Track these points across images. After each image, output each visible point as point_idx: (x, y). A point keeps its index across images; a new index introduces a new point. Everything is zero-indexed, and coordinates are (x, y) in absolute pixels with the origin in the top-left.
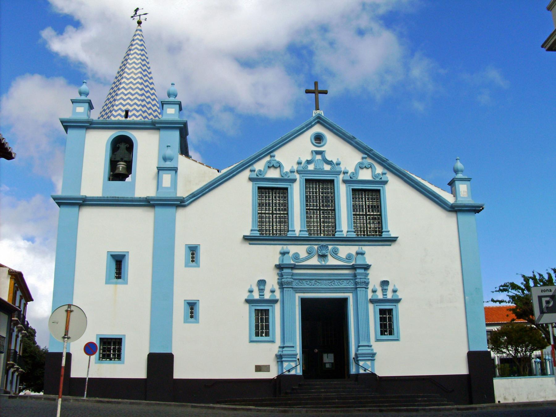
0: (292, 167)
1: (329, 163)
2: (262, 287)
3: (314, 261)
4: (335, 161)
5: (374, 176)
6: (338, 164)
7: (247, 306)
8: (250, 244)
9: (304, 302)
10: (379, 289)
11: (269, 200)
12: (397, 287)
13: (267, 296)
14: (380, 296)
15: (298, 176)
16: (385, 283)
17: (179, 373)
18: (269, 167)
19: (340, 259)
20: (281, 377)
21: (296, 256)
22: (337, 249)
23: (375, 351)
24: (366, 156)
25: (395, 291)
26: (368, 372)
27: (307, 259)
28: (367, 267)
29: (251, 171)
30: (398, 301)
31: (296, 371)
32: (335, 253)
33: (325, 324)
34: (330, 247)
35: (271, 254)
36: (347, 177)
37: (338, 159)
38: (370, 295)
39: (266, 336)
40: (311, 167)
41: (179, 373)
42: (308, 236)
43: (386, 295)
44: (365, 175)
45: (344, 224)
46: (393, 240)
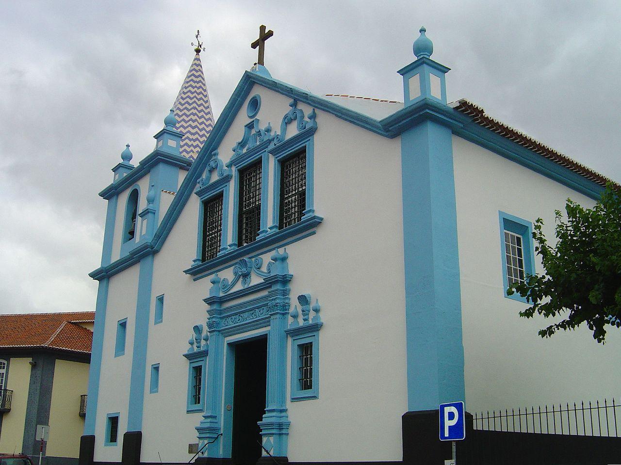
21: (226, 286)
27: (234, 283)
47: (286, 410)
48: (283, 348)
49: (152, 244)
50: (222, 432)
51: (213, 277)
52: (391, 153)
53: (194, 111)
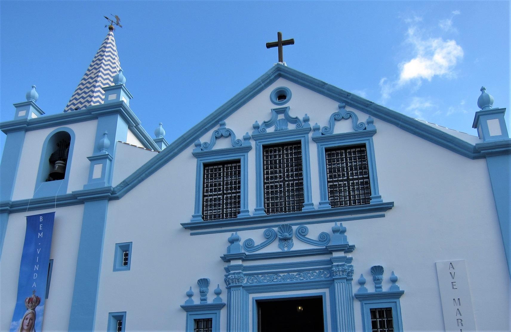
0: (247, 133)
1: (295, 120)
2: (204, 289)
3: (274, 248)
4: (301, 118)
5: (356, 127)
6: (306, 120)
7: (184, 314)
8: (192, 234)
9: (261, 304)
10: (369, 279)
12: (397, 275)
13: (211, 299)
14: (370, 289)
15: (253, 143)
16: (377, 270)
18: (216, 138)
19: (309, 242)
21: (249, 244)
22: (306, 229)
24: (344, 104)
25: (394, 281)
27: (263, 246)
28: (350, 249)
29: (196, 146)
30: (400, 294)
32: (302, 235)
34: (294, 228)
35: (217, 242)
36: (318, 134)
37: (306, 115)
38: (355, 289)
40: (270, 130)
43: (380, 287)
44: (343, 128)
45: (315, 193)
46: (389, 206)
48: (351, 309)
49: (116, 189)
51: (228, 235)
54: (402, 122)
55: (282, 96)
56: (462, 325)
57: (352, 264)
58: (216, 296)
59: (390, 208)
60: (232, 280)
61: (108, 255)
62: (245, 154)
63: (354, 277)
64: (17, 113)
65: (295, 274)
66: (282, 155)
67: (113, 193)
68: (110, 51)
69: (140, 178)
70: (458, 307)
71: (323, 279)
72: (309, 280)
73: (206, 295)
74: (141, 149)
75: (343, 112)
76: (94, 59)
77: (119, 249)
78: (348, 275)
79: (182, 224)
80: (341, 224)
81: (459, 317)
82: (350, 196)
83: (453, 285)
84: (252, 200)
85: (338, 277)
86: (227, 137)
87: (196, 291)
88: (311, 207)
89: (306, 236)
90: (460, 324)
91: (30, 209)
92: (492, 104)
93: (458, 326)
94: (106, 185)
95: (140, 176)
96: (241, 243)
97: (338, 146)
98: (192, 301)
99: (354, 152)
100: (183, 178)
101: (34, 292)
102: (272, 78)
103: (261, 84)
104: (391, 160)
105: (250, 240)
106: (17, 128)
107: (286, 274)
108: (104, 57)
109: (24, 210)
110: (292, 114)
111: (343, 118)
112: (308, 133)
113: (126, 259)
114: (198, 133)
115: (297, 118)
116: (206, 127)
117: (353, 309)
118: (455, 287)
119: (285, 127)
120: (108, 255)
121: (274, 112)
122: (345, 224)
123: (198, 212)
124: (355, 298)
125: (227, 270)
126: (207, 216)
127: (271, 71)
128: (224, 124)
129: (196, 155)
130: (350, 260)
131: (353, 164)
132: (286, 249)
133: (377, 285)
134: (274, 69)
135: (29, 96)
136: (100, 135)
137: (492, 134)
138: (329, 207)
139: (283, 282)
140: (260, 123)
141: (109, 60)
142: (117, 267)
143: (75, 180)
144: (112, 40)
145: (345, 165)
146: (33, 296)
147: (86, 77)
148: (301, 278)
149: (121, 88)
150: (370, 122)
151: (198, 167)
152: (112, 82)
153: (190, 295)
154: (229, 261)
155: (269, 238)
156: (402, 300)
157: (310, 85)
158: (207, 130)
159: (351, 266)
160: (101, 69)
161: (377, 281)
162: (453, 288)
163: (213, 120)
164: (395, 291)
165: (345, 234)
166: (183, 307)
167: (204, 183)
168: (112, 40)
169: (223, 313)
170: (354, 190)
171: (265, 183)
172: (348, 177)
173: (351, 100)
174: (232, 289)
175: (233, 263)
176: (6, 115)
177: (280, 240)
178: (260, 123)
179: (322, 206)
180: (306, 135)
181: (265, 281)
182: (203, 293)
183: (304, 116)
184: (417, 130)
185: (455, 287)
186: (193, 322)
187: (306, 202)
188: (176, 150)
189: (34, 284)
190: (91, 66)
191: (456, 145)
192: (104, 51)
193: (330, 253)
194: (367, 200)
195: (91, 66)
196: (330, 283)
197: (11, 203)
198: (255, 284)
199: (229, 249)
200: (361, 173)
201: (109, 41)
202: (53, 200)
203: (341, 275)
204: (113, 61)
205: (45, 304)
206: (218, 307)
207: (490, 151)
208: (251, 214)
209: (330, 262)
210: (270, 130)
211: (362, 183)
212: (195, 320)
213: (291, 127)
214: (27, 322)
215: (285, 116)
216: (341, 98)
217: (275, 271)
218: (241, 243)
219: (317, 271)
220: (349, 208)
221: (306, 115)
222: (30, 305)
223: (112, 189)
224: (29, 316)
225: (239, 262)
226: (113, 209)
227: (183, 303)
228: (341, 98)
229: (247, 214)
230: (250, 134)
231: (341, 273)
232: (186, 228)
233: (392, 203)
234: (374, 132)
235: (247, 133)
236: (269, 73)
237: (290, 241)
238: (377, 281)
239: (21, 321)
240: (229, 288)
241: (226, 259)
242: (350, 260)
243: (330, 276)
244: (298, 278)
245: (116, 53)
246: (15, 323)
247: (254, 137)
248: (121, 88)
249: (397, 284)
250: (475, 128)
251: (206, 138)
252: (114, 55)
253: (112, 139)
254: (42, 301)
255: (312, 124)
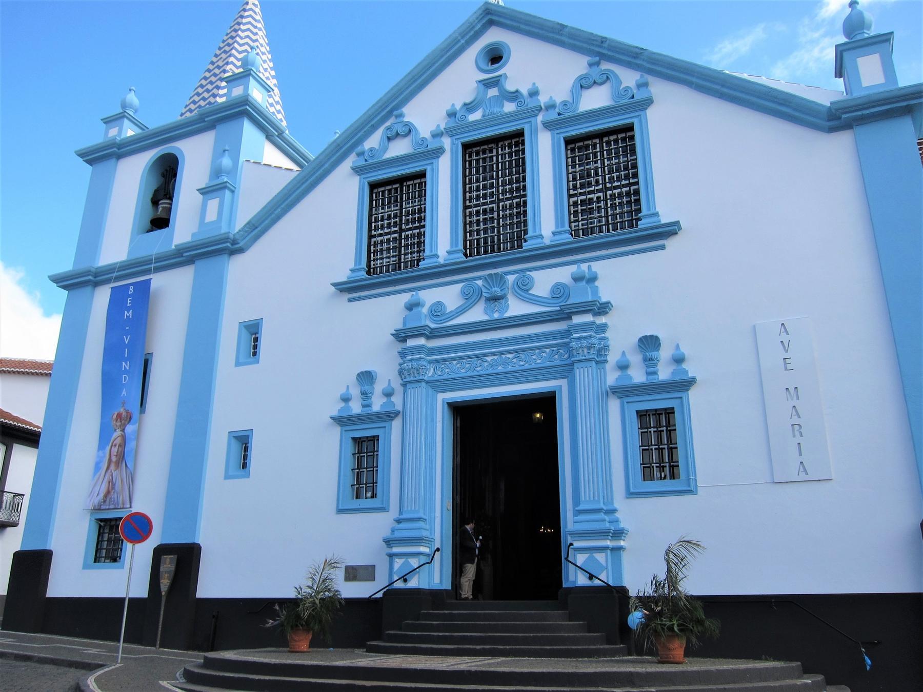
0: (438, 126)
1: (514, 96)
2: (366, 388)
3: (477, 314)
4: (524, 91)
5: (616, 95)
6: (534, 93)
7: (337, 430)
8: (350, 300)
9: (459, 410)
10: (635, 359)
11: (596, 162)
12: (685, 350)
13: (377, 404)
14: (638, 376)
15: (446, 142)
16: (649, 343)
17: (211, 585)
18: (389, 139)
19: (536, 300)
20: (391, 594)
21: (437, 310)
22: (530, 278)
23: (622, 525)
24: (597, 59)
25: (679, 360)
26: (597, 582)
27: (461, 311)
28: (603, 309)
29: (359, 155)
30: (686, 384)
31: (431, 575)
32: (524, 289)
33: (507, 458)
34: (511, 278)
35: (387, 310)
36: (553, 115)
37: (534, 84)
38: (612, 378)
39: (372, 497)
40: (476, 116)
41: (211, 585)
42: (571, 239)
43: (655, 373)
44: (596, 99)
45: (547, 215)
46: (671, 230)
47: (614, 511)
48: (604, 413)
49: (237, 237)
50: (438, 545)
51: (406, 298)
52: (840, 146)
53: (247, 40)
54: (698, 78)
55: (495, 57)
56: (801, 435)
57: (607, 335)
58: (385, 399)
59: (675, 233)
60: (409, 370)
61: (229, 340)
62: (435, 161)
63: (609, 358)
64: (107, 132)
65: (511, 356)
66: (494, 156)
67: (234, 242)
68: (249, 23)
69: (273, 216)
70: (795, 402)
71: (558, 362)
72: (533, 366)
73: (370, 398)
74: (276, 169)
75: (595, 73)
76: (225, 38)
77: (244, 330)
78: (599, 355)
79: (334, 285)
80: (590, 267)
81: (795, 420)
82: (607, 216)
83: (785, 364)
84: (443, 235)
85: (581, 358)
86: (406, 135)
87: (355, 392)
88: (539, 240)
89: (531, 292)
90: (797, 433)
91: (118, 279)
92: (869, 28)
93: (794, 436)
94: (224, 230)
95: (273, 213)
96: (425, 310)
97: (586, 133)
98: (349, 408)
99: (616, 141)
100: (338, 212)
101: (124, 403)
102: (477, 28)
103: (459, 41)
104: (679, 148)
105: (439, 304)
106: (101, 156)
107: (496, 357)
108: (240, 32)
109: (108, 281)
110: (510, 87)
111: (595, 82)
112: (536, 116)
113: (255, 347)
114: (359, 135)
115: (517, 91)
116: (373, 123)
117: (607, 412)
118: (789, 367)
119: (499, 110)
120: (229, 340)
121: (481, 86)
122: (597, 267)
123: (457, 245)
124: (610, 394)
125: (402, 355)
126: (577, 231)
127: (475, 17)
128: (401, 115)
129: (357, 170)
130: (603, 328)
131: (614, 161)
132: (496, 316)
133: (649, 370)
134: (480, 12)
135: (124, 106)
136: (219, 152)
137: (865, 84)
138: (567, 238)
139: (491, 371)
140: (458, 107)
141: (247, 37)
142: (242, 360)
143: (183, 230)
144: (254, 4)
145: (606, 163)
146: (122, 410)
147: (211, 67)
148: (522, 363)
149: (250, 75)
150: (642, 85)
151: (361, 190)
152: (237, 67)
153: (346, 399)
154: (404, 340)
155: (470, 298)
156: (694, 396)
157: (541, 32)
158: (375, 128)
159: (604, 338)
160: (234, 52)
161: (650, 363)
162: (786, 369)
163: (383, 110)
164: (678, 378)
165: (596, 283)
166: (334, 418)
167: (370, 215)
168: (254, 4)
169: (396, 424)
170: (613, 207)
171: (570, 196)
172: (605, 183)
173: (609, 50)
174: (408, 386)
175: (411, 343)
176: (96, 136)
177: (488, 300)
178: (458, 107)
179: (558, 237)
180: (532, 119)
181: (461, 370)
182: (365, 395)
183: (530, 86)
184: (725, 90)
185: (789, 367)
186: (350, 442)
187: (531, 233)
188: (327, 166)
189: (124, 392)
190: (220, 49)
191: (795, 109)
192: (239, 24)
193: (569, 317)
194: (519, 238)
195: (220, 49)
196: (567, 370)
197: (93, 270)
198: (446, 376)
199: (405, 321)
200: (627, 177)
201: (248, 7)
202: (149, 262)
203: (585, 354)
204: (254, 38)
205: (140, 422)
206: (388, 416)
207: (859, 113)
208: (547, 241)
209: (567, 333)
210: (476, 116)
211: (628, 194)
212: (354, 439)
213: (509, 107)
214: (115, 450)
215: (499, 90)
216: (592, 48)
217: (477, 353)
218: (425, 310)
219: (548, 350)
220: (510, 254)
221: (534, 84)
222: (118, 424)
223: (231, 236)
224: (118, 441)
225: (422, 341)
226: (236, 268)
227: (335, 413)
228: (592, 48)
229: (435, 260)
230: (442, 127)
231: (585, 350)
232: (341, 291)
233: (677, 223)
234: (649, 102)
235: (438, 126)
236: (471, 20)
237: (503, 301)
238: (650, 363)
239: (108, 448)
240: (404, 385)
241: (401, 336)
242: (603, 328)
243: (569, 357)
244: (516, 363)
245: (259, 25)
246: (101, 452)
247: (449, 132)
248: (250, 75)
249: (684, 366)
250: (840, 76)
251: (373, 142)
252: (256, 27)
253: (236, 159)
254: (136, 415)
255: (543, 99)
